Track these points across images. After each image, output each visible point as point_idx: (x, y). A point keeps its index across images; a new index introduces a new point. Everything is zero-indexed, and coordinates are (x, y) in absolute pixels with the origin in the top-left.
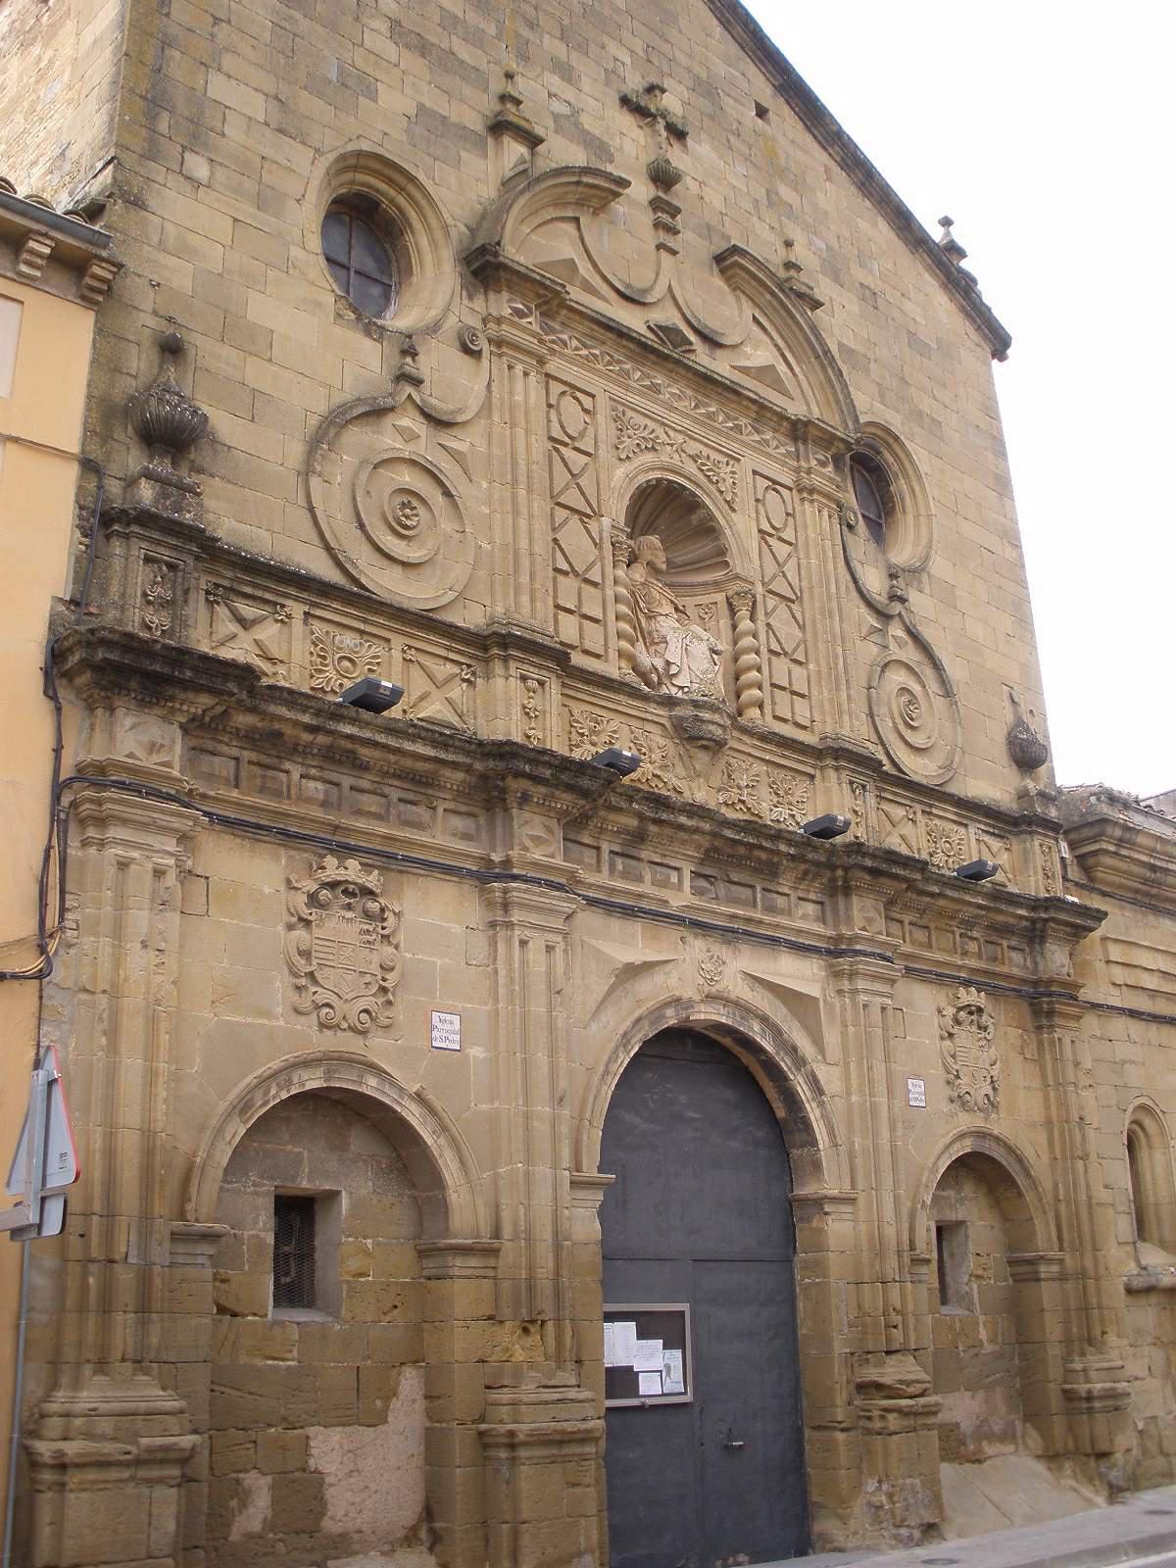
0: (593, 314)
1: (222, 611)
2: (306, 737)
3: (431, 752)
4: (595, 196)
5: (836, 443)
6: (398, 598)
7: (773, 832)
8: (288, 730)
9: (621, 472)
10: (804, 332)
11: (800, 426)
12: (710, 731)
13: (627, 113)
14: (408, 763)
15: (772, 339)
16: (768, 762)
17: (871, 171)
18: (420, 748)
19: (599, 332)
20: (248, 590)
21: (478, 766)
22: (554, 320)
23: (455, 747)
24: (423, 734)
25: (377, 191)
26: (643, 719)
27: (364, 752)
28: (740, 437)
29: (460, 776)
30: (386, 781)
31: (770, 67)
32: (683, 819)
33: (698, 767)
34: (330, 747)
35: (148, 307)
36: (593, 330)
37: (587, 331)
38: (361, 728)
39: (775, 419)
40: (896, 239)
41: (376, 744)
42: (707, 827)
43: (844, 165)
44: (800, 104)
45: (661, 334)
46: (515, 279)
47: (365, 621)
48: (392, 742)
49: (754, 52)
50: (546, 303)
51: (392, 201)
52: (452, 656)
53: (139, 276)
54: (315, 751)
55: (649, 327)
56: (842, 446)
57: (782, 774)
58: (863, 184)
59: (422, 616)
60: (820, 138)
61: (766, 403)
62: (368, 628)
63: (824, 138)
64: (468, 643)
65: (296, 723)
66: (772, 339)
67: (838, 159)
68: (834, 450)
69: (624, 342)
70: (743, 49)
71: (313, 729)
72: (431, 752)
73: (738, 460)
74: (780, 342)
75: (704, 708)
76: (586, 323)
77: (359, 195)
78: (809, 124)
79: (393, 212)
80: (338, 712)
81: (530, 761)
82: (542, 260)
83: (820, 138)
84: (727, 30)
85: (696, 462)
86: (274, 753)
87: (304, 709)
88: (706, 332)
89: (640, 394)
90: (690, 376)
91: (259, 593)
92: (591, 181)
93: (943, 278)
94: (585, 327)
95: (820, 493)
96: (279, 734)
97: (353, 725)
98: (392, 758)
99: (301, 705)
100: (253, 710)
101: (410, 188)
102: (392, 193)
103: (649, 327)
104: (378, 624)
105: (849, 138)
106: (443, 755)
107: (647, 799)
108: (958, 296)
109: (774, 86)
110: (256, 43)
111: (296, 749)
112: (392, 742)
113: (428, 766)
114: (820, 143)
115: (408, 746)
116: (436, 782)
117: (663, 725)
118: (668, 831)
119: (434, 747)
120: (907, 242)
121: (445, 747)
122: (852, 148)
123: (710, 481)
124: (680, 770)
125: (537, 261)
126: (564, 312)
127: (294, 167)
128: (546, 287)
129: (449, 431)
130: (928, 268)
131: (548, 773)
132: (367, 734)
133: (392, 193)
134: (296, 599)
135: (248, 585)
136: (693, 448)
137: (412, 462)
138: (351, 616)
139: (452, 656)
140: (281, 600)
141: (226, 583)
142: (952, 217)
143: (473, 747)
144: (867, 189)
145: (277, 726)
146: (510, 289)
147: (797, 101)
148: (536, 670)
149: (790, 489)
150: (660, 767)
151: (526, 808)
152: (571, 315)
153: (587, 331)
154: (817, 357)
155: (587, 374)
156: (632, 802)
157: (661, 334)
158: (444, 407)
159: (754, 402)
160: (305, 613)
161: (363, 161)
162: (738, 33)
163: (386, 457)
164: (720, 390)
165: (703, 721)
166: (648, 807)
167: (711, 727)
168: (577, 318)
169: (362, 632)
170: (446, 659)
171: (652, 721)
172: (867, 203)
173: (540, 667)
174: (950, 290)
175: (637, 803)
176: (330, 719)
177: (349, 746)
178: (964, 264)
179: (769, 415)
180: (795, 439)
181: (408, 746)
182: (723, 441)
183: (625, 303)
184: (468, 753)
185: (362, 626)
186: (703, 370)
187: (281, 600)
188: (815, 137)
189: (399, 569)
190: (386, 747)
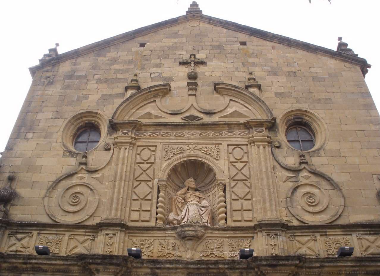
0: (152, 124)
1: (317, 253)
2: (24, 266)
3: (62, 262)
4: (159, 92)
5: (264, 123)
6: (68, 222)
7: (213, 262)
8: (19, 266)
9: (165, 164)
10: (248, 96)
11: (246, 124)
12: (188, 234)
13: (182, 66)
14: (58, 267)
15: (240, 103)
16: (228, 237)
17: (289, 39)
18: (58, 262)
19: (158, 128)
20: (21, 231)
21: (79, 264)
22: (141, 130)
23: (70, 260)
24: (57, 258)
25: (90, 120)
26: (166, 236)
27: (42, 267)
28: (223, 137)
29: (76, 268)
30: (54, 274)
31: (245, 31)
32: (168, 266)
33: (188, 247)
34: (33, 268)
35: (8, 172)
36: (155, 128)
37: (154, 129)
38: (38, 260)
39: (236, 126)
40: (307, 53)
41: (45, 264)
42: (181, 266)
43: (280, 43)
44: (259, 35)
45: (186, 119)
46: (121, 125)
47: (57, 231)
48: (49, 262)
49: (239, 30)
50: (135, 127)
51: (95, 121)
52: (87, 234)
53: (7, 165)
54: (29, 269)
55: (182, 119)
56: (267, 123)
57: (235, 240)
58: (289, 44)
59: (77, 225)
60: (269, 40)
61: (229, 123)
62: (58, 233)
63: (270, 39)
64: (91, 229)
65: (20, 263)
66: (240, 103)
67: (277, 42)
68: (265, 126)
69: (167, 127)
70: (235, 31)
71: (25, 263)
72: (62, 262)
73: (221, 144)
74: (147, 102)
75: (185, 227)
76: (152, 127)
77: (86, 123)
78: (264, 38)
79: (96, 123)
80: (29, 257)
81: (92, 259)
82: (139, 116)
83: (269, 40)
84: (229, 29)
85: (200, 150)
86: (18, 272)
87: (20, 259)
88: (207, 112)
89: (175, 139)
90: (196, 126)
91: (24, 231)
92: (154, 89)
93: (330, 55)
94: (152, 128)
95: (257, 141)
96: (16, 267)
97: (36, 260)
98: (52, 267)
99: (18, 258)
100: (5, 262)
101: (98, 116)
102: (94, 119)
103: (182, 119)
104: (61, 231)
105: (277, 35)
106: (66, 263)
107: (147, 262)
108: (338, 57)
109: (249, 35)
110: (53, 102)
111: (24, 270)
112: (49, 262)
113: (64, 267)
114: (270, 41)
115: (54, 262)
116: (70, 271)
117: (174, 236)
118: (165, 271)
119: (63, 261)
120: (312, 52)
121: (67, 260)
122: (279, 36)
123: (207, 154)
124: (182, 249)
125: (136, 118)
126: (143, 127)
127: (58, 125)
128: (132, 123)
129: (97, 173)
130: (323, 55)
131: (99, 261)
132: (40, 261)
133: (94, 119)
134: (35, 230)
135: (21, 230)
136: (200, 147)
137: (80, 185)
138: (53, 231)
139: (87, 234)
140: (31, 231)
141: (15, 231)
142: (340, 36)
143: (76, 258)
144: (290, 45)
145: (15, 265)
146: (122, 128)
147: (257, 35)
148: (112, 231)
149: (247, 145)
150: (172, 250)
151: (100, 273)
152: (146, 127)
153: (154, 129)
154: (255, 101)
155: (153, 141)
156: (143, 264)
157: (186, 119)
158: (96, 167)
159: (225, 124)
160: (38, 233)
161: (83, 115)
162: (232, 28)
163: (74, 184)
164: (209, 126)
165: (185, 231)
166: (151, 264)
167: (188, 232)
168: (148, 127)
169: (57, 234)
170: (85, 235)
171: (169, 236)
172: (292, 48)
173: (113, 230)
174: (334, 57)
175: (145, 264)
176: (28, 260)
177: (38, 266)
178: (349, 47)
179: (233, 126)
180: (248, 129)
181: (54, 262)
182: (213, 141)
183: (173, 116)
184: (75, 261)
185: (56, 232)
186: (235, 123)
187: (31, 231)
188: (268, 41)
189: (72, 214)
190: (48, 264)
